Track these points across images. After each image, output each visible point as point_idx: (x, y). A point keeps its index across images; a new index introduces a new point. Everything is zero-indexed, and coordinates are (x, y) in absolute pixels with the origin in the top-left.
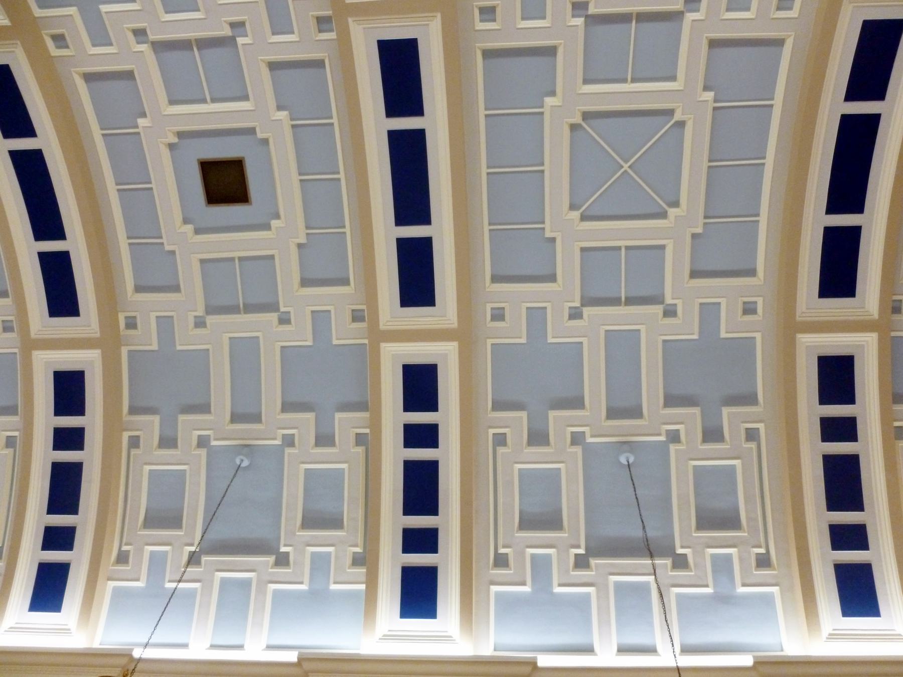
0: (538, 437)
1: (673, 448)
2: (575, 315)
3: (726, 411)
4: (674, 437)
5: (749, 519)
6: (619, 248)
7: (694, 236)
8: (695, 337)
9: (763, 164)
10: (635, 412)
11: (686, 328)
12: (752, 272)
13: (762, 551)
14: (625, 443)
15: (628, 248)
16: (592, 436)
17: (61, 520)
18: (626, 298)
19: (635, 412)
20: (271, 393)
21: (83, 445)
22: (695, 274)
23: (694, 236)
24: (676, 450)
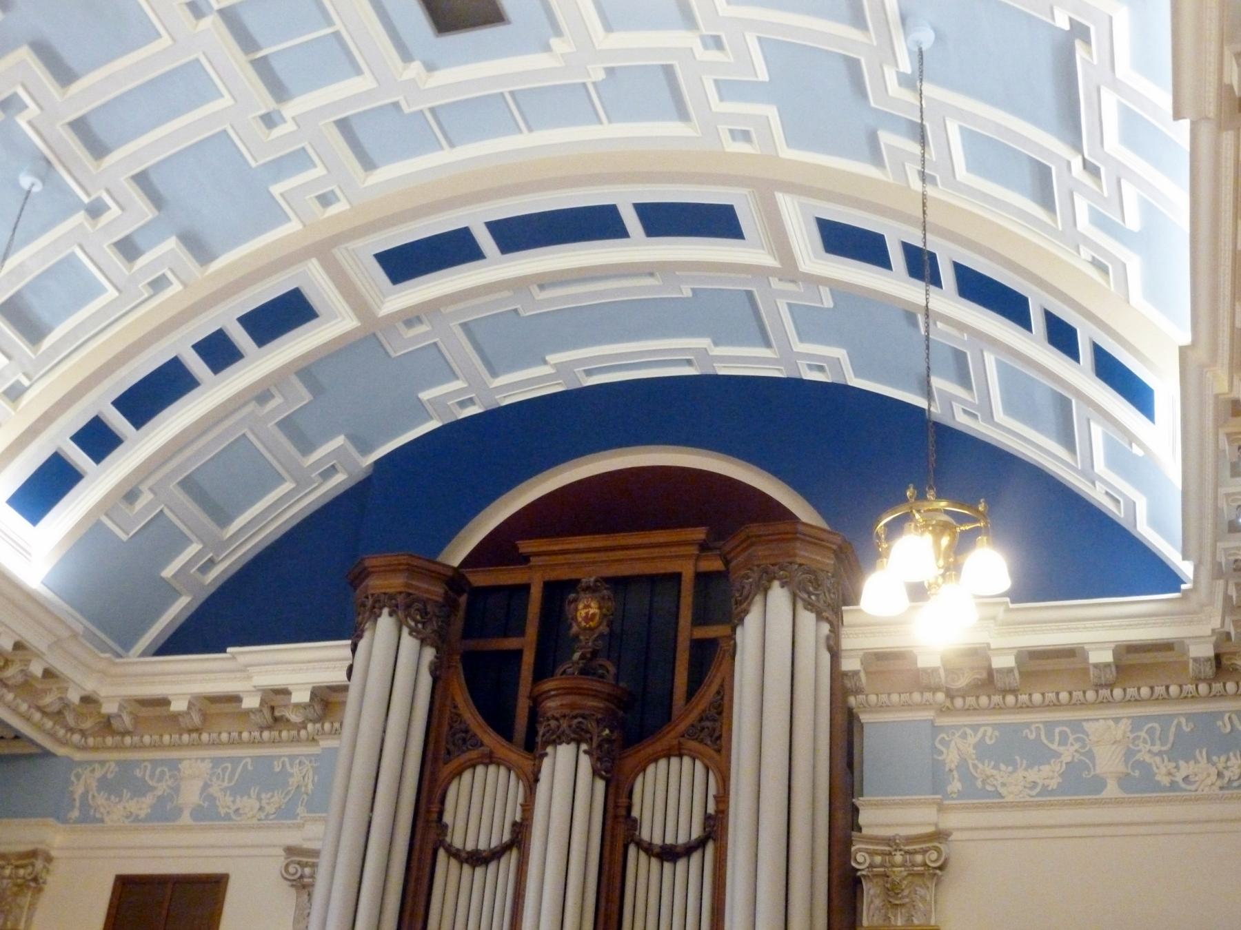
0: (128, 248)
1: (80, 217)
2: (269, 120)
3: (172, 243)
4: (96, 210)
5: (54, 348)
6: (330, 22)
7: (396, 105)
8: (253, 164)
9: (520, 131)
10: (98, 149)
11: (257, 148)
12: (369, 165)
13: (26, 382)
14: (48, 162)
15: (337, 35)
16: (30, 123)
17: (118, 422)
18: (265, 58)
19: (98, 149)
20: (131, 155)
21: (197, 351)
22: (344, 125)
23: (396, 105)
24: (81, 225)
